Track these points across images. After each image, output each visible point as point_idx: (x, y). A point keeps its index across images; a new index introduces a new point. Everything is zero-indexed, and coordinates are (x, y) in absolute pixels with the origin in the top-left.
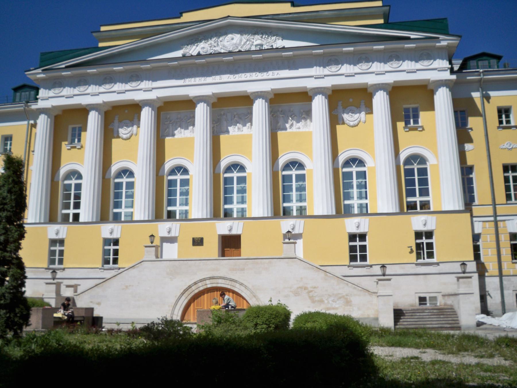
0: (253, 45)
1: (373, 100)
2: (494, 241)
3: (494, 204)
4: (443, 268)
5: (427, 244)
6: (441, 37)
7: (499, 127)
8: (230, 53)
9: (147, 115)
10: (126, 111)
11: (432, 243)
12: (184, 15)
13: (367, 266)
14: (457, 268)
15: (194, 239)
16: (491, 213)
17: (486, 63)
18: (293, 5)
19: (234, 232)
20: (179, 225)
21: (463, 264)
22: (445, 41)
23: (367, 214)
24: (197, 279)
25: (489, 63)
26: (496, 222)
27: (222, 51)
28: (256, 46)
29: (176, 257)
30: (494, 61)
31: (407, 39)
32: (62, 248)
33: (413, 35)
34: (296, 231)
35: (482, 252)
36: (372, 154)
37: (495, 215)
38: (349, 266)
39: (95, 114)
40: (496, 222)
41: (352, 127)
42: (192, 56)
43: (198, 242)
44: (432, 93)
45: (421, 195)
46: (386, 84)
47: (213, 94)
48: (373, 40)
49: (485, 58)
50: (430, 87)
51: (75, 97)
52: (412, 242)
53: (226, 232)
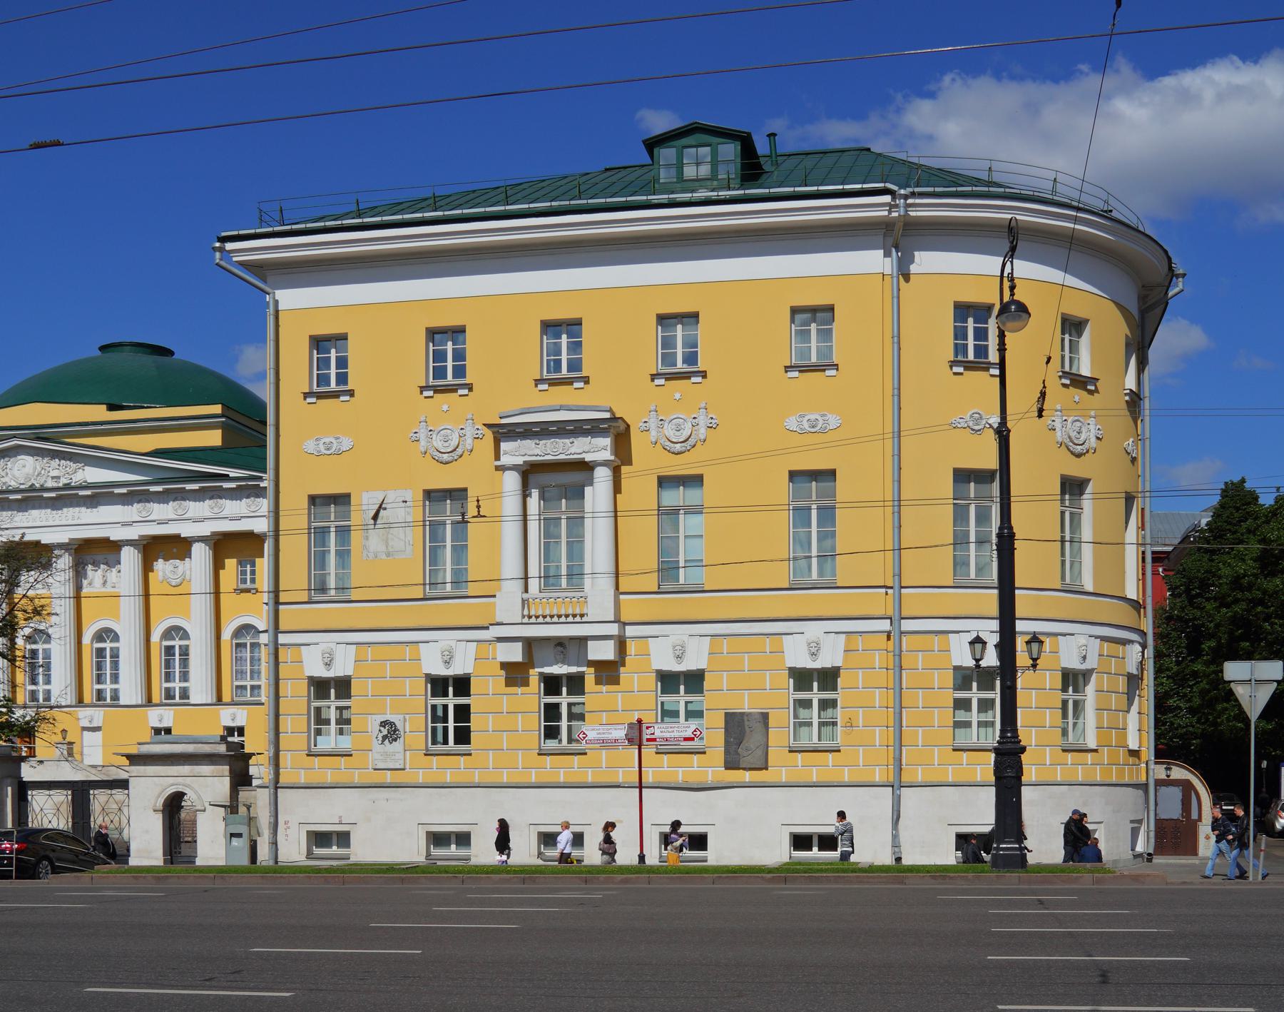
0: (48, 476)
2: (1058, 708)
10: (175, 550)
20: (103, 712)
31: (225, 477)
33: (233, 473)
39: (129, 550)
41: (174, 586)
51: (243, 520)
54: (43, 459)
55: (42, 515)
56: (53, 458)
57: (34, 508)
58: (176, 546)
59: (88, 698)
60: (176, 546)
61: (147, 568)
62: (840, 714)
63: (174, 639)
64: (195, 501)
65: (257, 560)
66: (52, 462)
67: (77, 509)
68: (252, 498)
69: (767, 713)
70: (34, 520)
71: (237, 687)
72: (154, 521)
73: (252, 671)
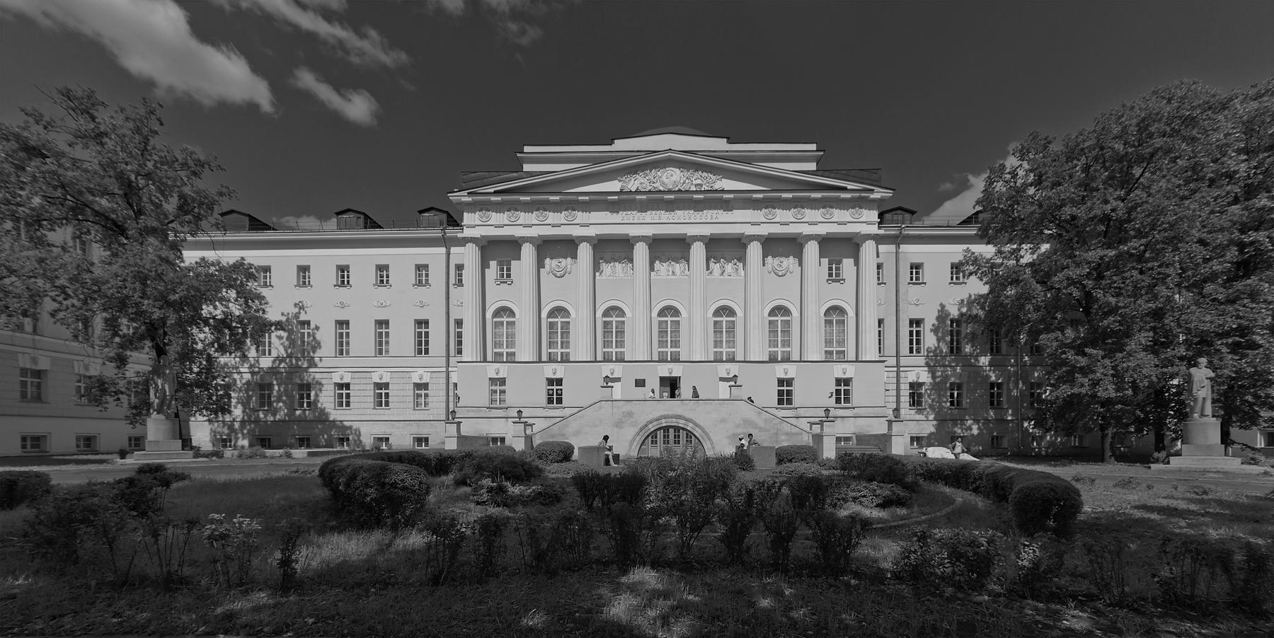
1: (692, 250)
3: (898, 356)
6: (876, 189)
7: (879, 284)
8: (670, 192)
9: (585, 251)
10: (559, 247)
13: (794, 408)
16: (894, 363)
26: (898, 373)
27: (662, 189)
28: (696, 185)
30: (907, 216)
31: (844, 189)
32: (387, 391)
33: (850, 186)
37: (898, 366)
40: (898, 373)
41: (559, 277)
43: (640, 383)
45: (783, 346)
50: (856, 240)
52: (833, 388)
55: (624, 215)
61: (540, 264)
62: (430, 399)
64: (497, 213)
67: (716, 211)
68: (857, 208)
69: (671, 397)
72: (493, 225)
73: (562, 343)
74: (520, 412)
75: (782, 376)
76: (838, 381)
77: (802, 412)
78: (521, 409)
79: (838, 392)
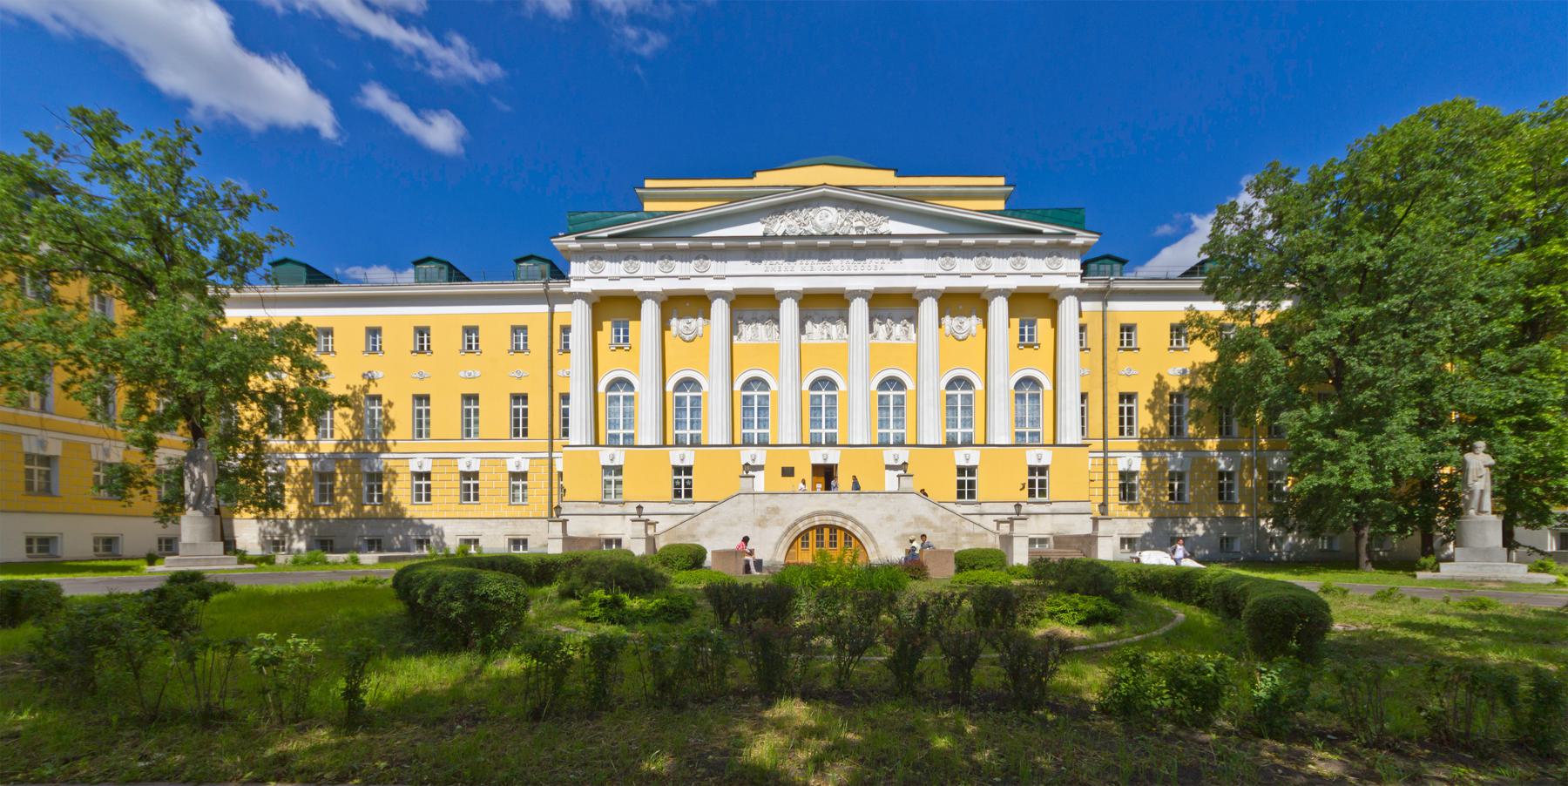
4: (986, 508)
5: (686, 480)
6: (1079, 233)
8: (824, 236)
11: (974, 481)
12: (758, 174)
14: (1011, 508)
15: (783, 469)
17: (1108, 268)
18: (899, 174)
19: (830, 461)
21: (1018, 506)
22: (1081, 238)
23: (767, 445)
24: (846, 512)
25: (1112, 268)
27: (815, 232)
28: (857, 228)
29: (763, 490)
30: (1117, 266)
31: (1039, 233)
33: (1046, 229)
34: (758, 462)
35: (1217, 492)
36: (707, 375)
37: (1105, 450)
38: (956, 503)
42: (776, 236)
43: (788, 472)
44: (847, 304)
46: (866, 291)
47: (664, 291)
48: (988, 232)
49: (1107, 261)
51: (974, 277)
52: (1026, 478)
53: (820, 461)
54: (801, 210)
56: (857, 210)
57: (835, 257)
58: (694, 303)
59: (670, 441)
60: (694, 303)
61: (665, 326)
62: (528, 492)
63: (685, 391)
65: (631, 323)
66: (857, 214)
67: (881, 260)
70: (835, 269)
71: (610, 435)
73: (692, 422)
74: (640, 508)
75: (963, 463)
76: (1032, 470)
77: (986, 508)
78: (642, 504)
79: (1031, 483)
